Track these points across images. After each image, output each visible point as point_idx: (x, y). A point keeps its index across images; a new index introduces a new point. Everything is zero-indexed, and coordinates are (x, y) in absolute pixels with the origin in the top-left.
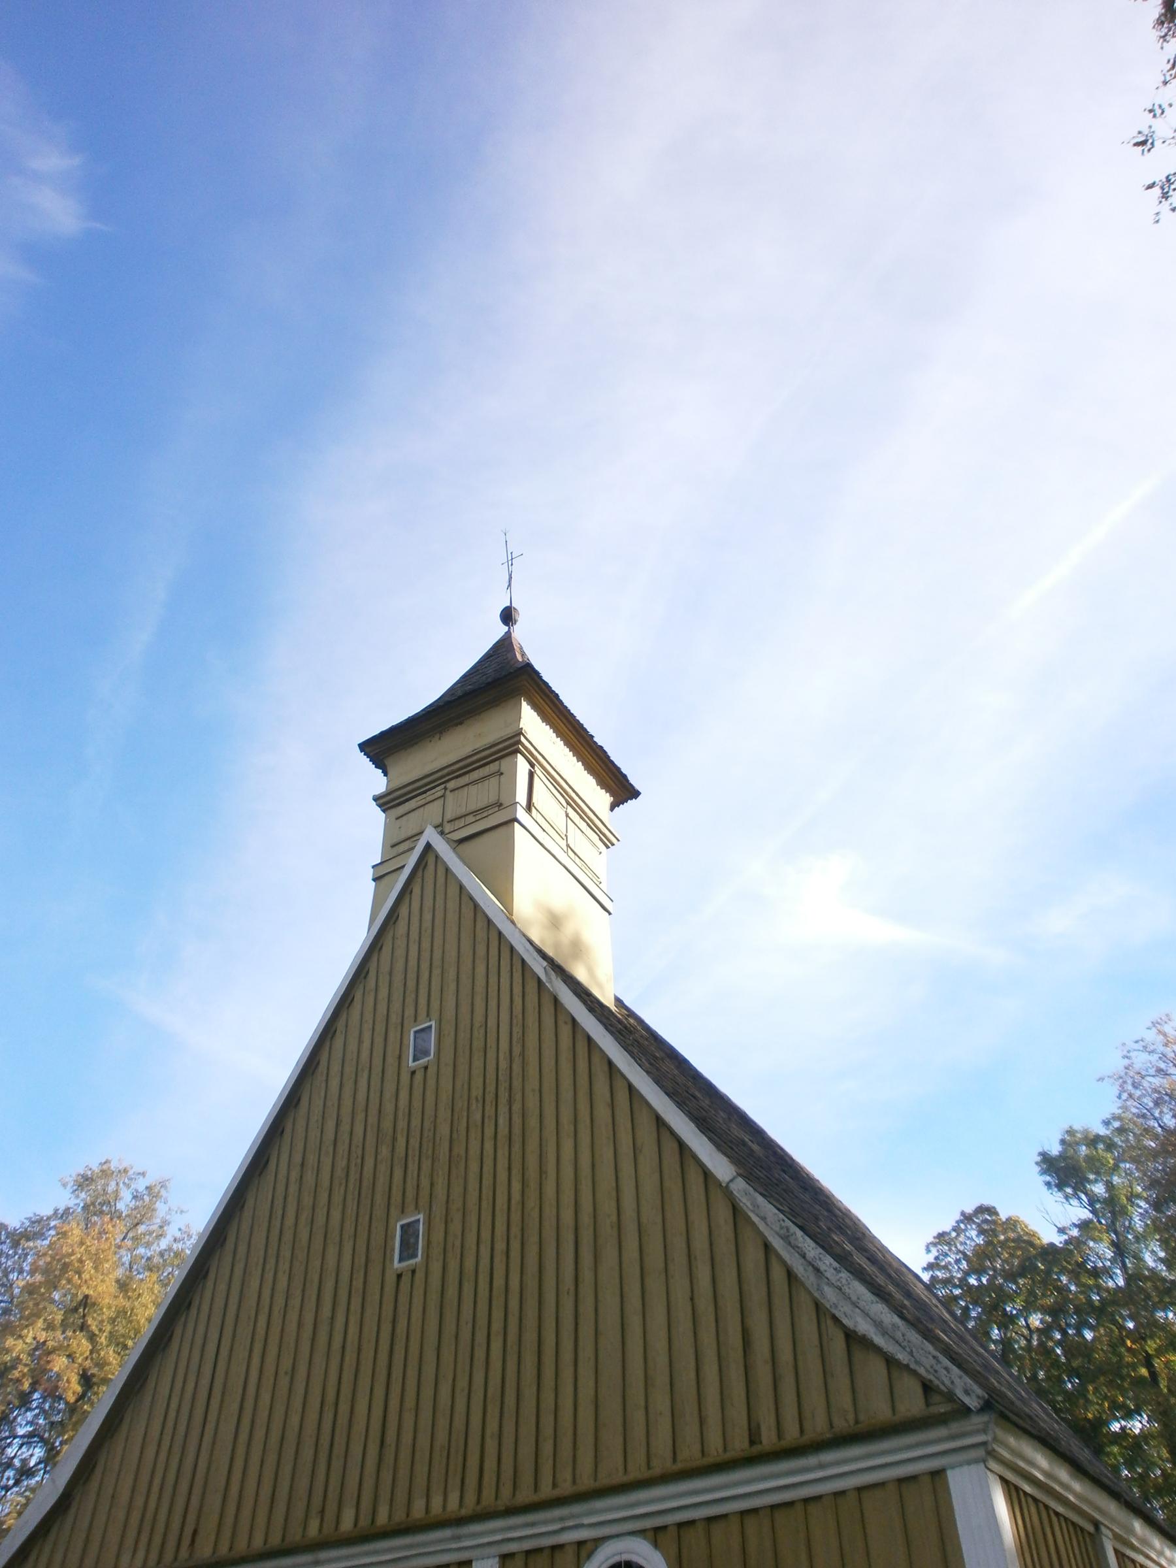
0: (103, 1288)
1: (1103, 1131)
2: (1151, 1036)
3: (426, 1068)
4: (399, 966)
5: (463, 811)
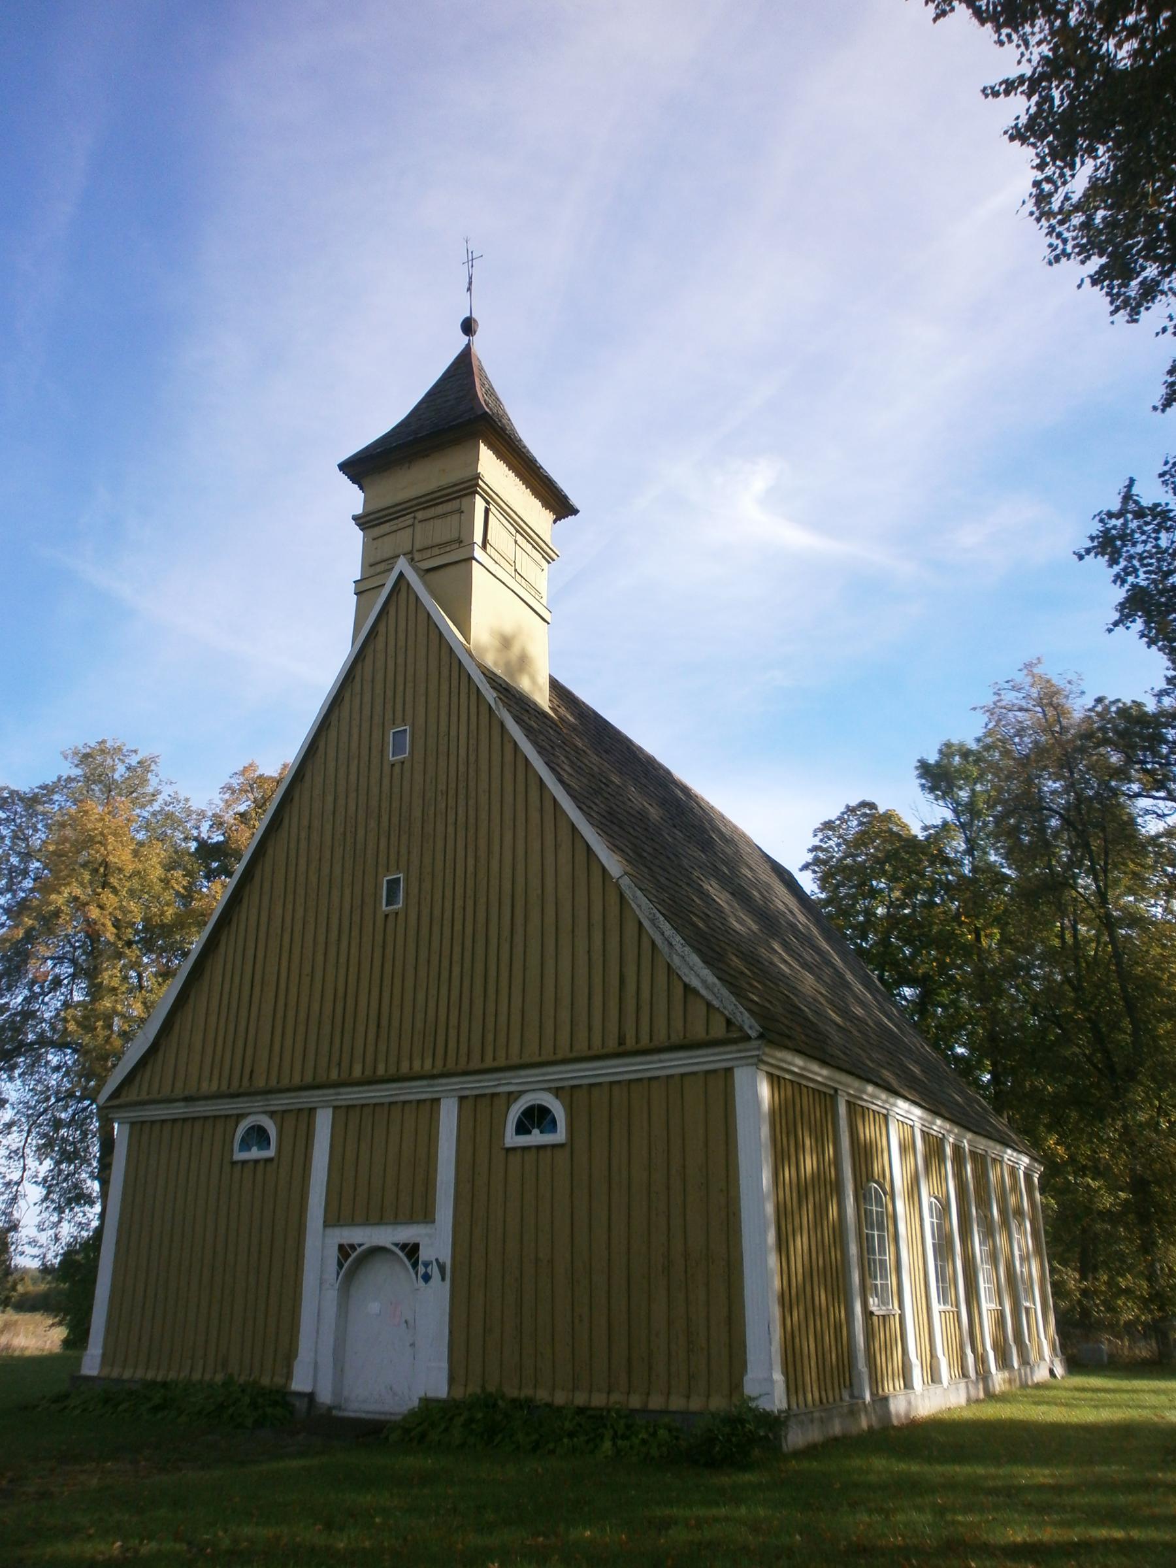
0: (122, 857)
1: (974, 746)
2: (1021, 678)
3: (403, 763)
4: (380, 676)
5: (430, 543)
